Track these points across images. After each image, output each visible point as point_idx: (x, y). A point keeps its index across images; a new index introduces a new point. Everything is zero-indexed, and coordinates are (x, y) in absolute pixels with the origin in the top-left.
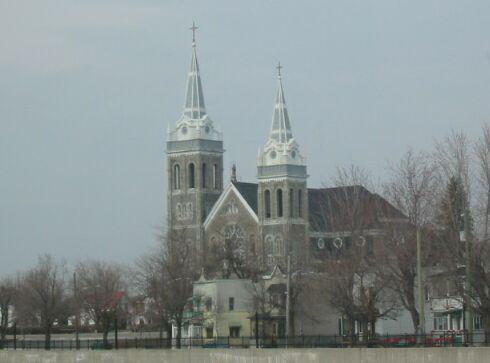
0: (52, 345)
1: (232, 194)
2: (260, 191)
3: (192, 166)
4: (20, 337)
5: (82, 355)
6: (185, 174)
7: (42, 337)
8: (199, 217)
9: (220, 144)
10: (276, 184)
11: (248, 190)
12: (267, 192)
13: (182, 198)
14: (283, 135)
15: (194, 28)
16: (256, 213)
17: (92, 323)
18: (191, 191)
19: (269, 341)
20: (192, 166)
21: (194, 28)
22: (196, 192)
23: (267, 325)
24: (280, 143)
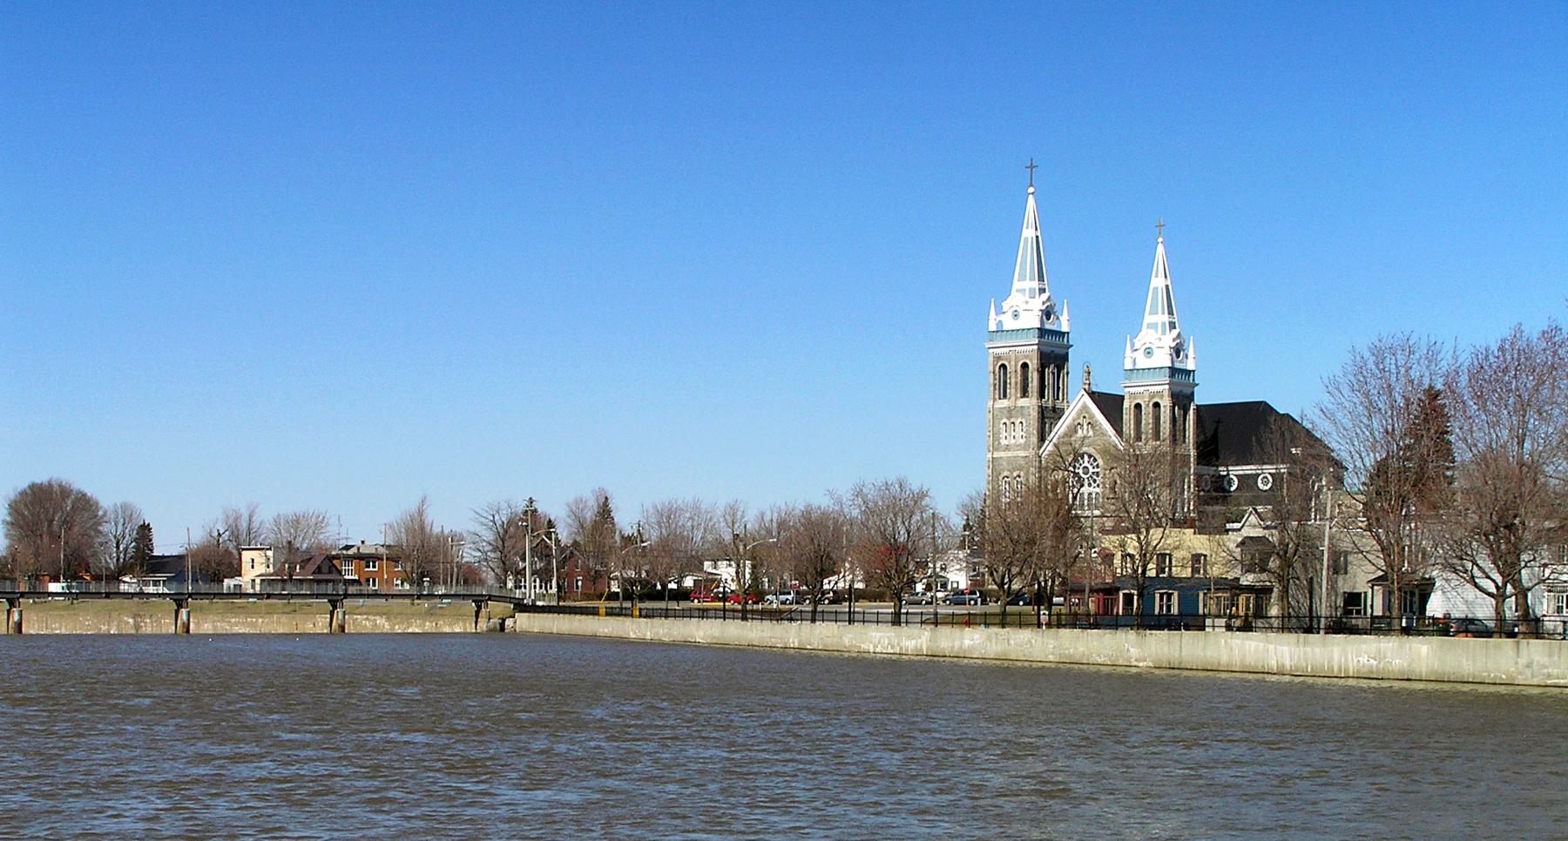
0: (903, 618)
1: (1085, 407)
2: (1126, 404)
3: (1025, 366)
4: (860, 606)
5: (976, 636)
6: (1014, 379)
7: (887, 608)
8: (1034, 439)
9: (1202, 628)
10: (1153, 395)
11: (1110, 405)
12: (1138, 406)
13: (1010, 412)
14: (1164, 324)
15: (1032, 167)
16: (1119, 432)
17: (860, 586)
18: (1023, 402)
19: (1238, 623)
20: (1025, 366)
21: (1032, 167)
22: (1031, 403)
23: (231, 546)
24: (1159, 334)
